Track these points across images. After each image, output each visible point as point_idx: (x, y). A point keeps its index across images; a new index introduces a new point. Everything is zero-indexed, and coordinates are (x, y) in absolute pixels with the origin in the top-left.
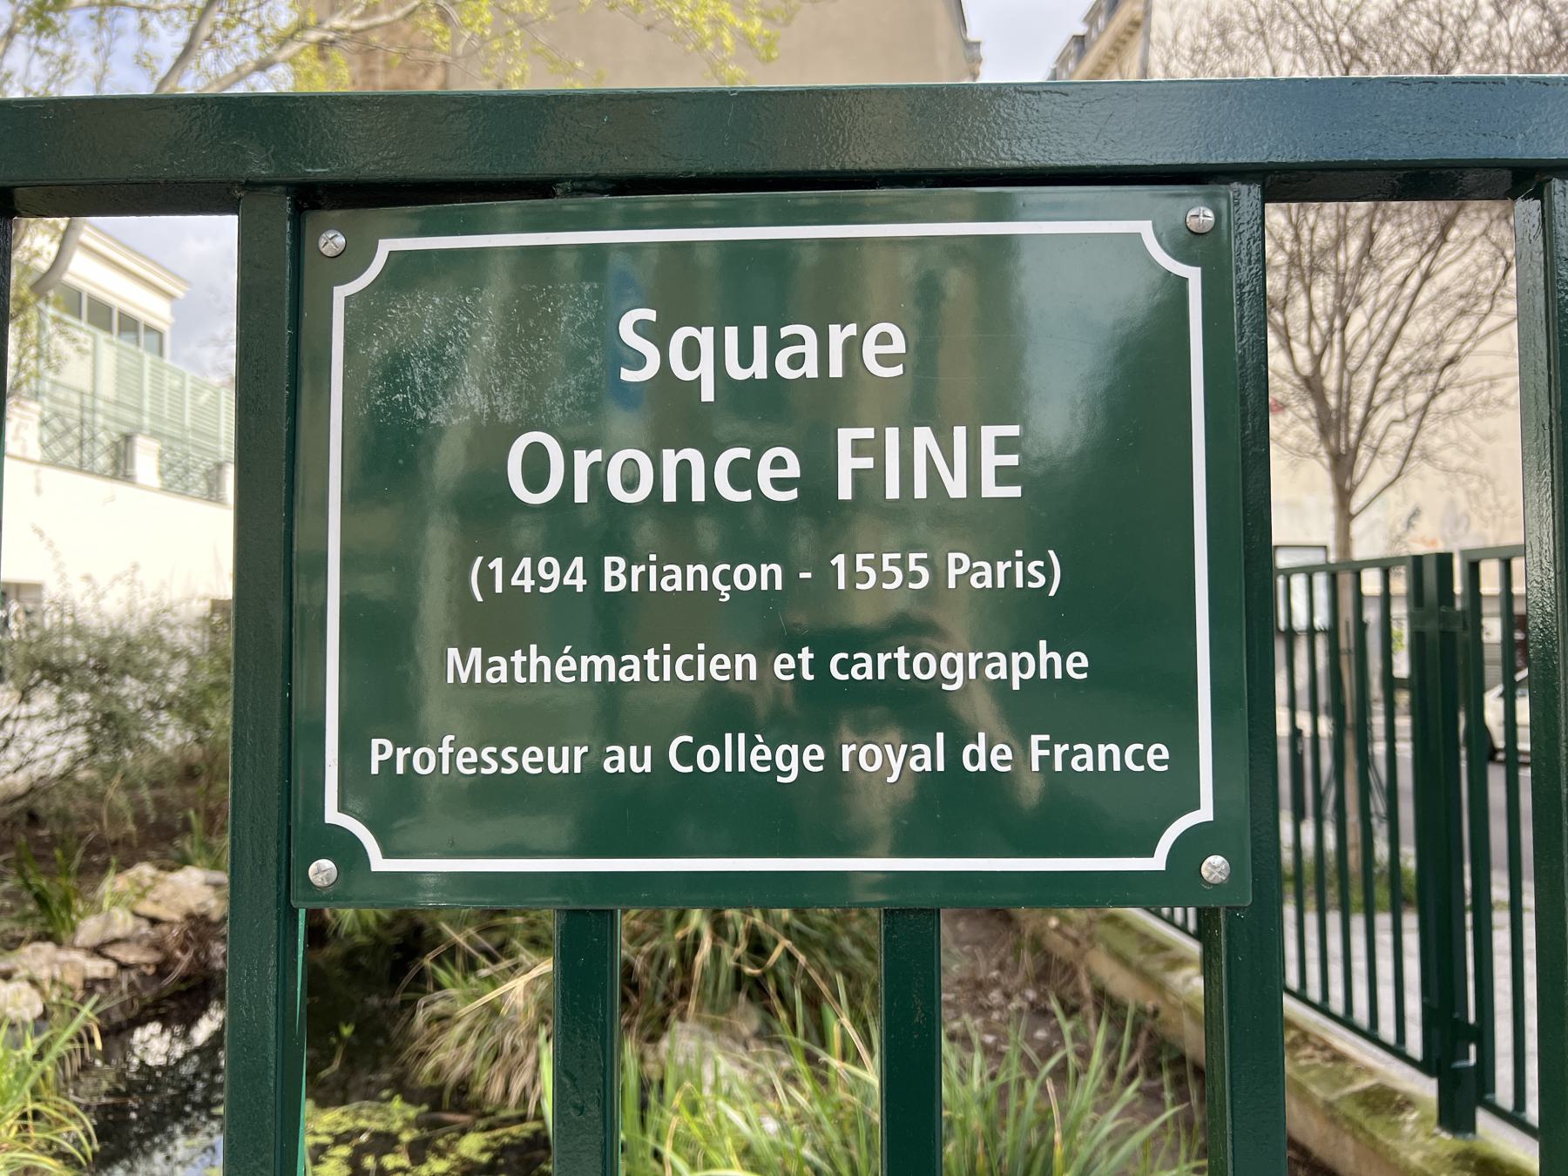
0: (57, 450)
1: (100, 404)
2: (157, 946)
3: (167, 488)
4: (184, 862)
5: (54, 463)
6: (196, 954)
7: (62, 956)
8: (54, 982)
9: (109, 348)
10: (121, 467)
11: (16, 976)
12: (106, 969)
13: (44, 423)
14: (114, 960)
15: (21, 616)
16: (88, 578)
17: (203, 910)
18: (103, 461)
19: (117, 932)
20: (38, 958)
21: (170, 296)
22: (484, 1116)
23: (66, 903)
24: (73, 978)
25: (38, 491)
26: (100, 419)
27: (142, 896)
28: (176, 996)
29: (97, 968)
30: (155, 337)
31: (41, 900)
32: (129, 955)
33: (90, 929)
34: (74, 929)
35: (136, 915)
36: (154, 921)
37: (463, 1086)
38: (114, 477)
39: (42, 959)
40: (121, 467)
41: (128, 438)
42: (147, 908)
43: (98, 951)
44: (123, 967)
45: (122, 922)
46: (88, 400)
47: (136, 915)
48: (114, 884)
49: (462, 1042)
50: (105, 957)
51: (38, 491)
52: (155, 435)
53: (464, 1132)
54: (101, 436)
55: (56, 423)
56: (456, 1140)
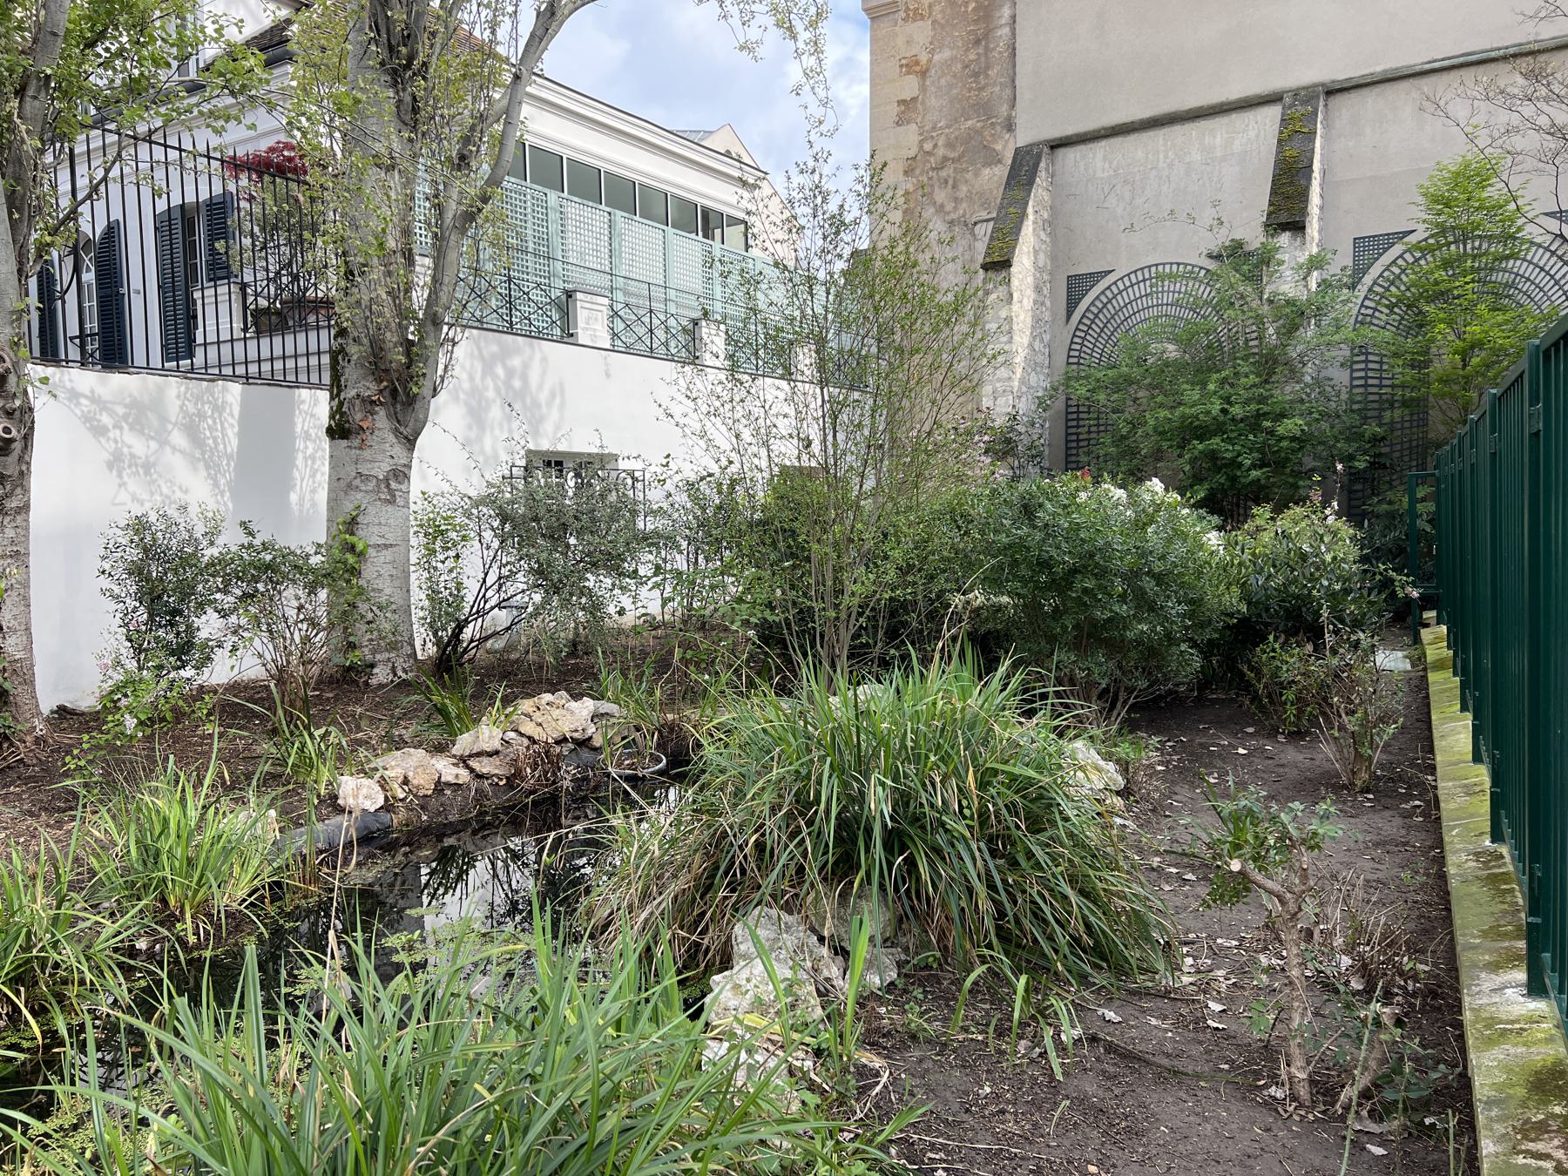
25: (608, 375)
33: (464, 744)
44: (480, 776)
46: (658, 293)
51: (608, 375)
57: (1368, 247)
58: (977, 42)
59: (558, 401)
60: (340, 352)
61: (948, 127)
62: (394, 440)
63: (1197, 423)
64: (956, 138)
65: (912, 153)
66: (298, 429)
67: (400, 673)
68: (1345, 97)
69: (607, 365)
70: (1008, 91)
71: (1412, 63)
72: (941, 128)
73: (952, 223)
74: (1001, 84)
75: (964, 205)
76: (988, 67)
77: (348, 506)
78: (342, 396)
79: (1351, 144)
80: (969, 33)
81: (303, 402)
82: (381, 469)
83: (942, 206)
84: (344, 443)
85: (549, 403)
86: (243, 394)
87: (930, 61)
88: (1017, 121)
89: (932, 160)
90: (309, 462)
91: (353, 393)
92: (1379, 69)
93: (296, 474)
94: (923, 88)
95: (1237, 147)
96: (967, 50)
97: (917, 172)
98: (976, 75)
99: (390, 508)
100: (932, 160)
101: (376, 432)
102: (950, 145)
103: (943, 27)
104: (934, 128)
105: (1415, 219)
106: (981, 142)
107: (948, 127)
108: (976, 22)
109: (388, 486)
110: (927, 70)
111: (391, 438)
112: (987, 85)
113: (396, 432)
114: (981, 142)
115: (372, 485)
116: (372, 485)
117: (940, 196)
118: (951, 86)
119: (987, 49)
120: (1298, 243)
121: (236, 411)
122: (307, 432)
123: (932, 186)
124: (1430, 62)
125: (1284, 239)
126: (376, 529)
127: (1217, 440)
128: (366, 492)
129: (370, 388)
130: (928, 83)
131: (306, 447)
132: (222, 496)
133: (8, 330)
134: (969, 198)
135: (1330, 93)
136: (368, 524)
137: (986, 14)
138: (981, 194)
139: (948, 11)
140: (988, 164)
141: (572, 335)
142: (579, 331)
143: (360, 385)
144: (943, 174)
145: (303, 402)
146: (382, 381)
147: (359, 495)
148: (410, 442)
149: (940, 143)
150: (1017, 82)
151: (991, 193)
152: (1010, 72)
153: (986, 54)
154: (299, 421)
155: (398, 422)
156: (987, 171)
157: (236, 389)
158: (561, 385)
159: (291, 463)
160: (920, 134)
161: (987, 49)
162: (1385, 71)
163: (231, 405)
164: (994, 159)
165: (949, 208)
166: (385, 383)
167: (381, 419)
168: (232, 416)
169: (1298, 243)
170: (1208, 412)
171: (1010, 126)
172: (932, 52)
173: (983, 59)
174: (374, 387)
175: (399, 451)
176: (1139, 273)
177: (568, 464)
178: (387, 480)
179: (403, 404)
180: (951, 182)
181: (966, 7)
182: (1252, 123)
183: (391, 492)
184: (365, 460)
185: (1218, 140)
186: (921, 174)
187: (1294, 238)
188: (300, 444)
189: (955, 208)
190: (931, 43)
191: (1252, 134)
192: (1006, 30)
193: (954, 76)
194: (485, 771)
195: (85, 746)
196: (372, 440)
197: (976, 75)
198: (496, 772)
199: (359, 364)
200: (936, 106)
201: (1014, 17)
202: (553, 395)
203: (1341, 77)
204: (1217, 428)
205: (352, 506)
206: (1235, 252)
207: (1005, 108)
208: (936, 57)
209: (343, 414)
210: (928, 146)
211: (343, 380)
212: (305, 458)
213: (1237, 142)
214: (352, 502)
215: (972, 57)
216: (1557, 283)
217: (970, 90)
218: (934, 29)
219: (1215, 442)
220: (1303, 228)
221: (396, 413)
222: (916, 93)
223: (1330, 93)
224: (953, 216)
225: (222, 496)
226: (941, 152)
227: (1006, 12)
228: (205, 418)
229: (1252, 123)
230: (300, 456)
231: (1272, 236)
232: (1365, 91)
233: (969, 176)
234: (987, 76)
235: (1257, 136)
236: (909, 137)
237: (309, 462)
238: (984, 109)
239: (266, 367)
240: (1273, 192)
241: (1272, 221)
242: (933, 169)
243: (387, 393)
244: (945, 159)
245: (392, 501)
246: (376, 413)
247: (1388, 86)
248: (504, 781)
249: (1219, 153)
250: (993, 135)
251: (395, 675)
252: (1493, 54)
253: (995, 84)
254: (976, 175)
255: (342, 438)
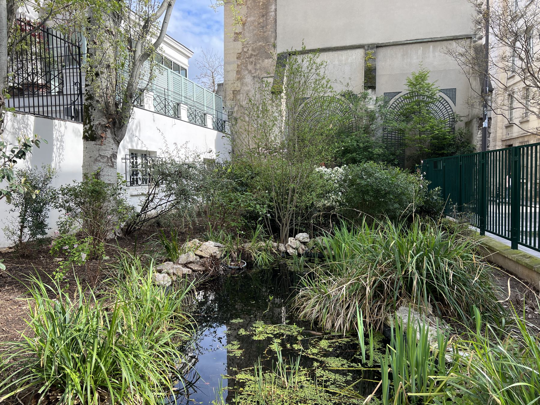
0: (159, 108)
1: (170, 93)
2: (203, 265)
3: (190, 122)
4: (207, 240)
5: (158, 113)
6: (215, 268)
7: (175, 266)
8: (174, 274)
9: (170, 73)
10: (177, 116)
11: (163, 272)
12: (189, 271)
13: (155, 99)
14: (191, 268)
15: (151, 162)
16: (175, 144)
17: (215, 254)
18: (172, 112)
19: (191, 260)
20: (168, 266)
21: (189, 57)
22: (326, 334)
23: (175, 249)
24: (180, 274)
25: (154, 121)
26: (170, 98)
27: (197, 249)
28: (210, 281)
29: (186, 271)
30: (185, 71)
31: (167, 247)
32: (196, 268)
33: (183, 258)
34: (178, 258)
35: (196, 255)
36: (201, 257)
37: (316, 322)
38: (174, 118)
39: (169, 267)
40: (177, 116)
41: (178, 105)
42: (198, 252)
43: (185, 265)
44: (194, 271)
45: (192, 257)
46: (166, 91)
47: (196, 255)
48: (189, 244)
49: (314, 306)
50: (188, 267)
51: (154, 121)
52: (186, 104)
53: (321, 339)
54: (170, 104)
55: (158, 99)
56: (318, 341)
57: (389, 95)
58: (263, 16)
59: (138, 128)
60: (90, 106)
61: (253, 44)
62: (113, 142)
63: (349, 148)
64: (256, 48)
65: (239, 52)
66: (54, 136)
67: (117, 234)
68: (384, 49)
69: (154, 117)
70: (274, 34)
71: (401, 40)
72: (250, 44)
73: (254, 77)
74: (271, 31)
75: (259, 71)
76: (267, 25)
77: (95, 168)
78: (92, 124)
79: (383, 64)
80: (260, 12)
81: (56, 125)
82: (109, 154)
83: (251, 71)
84: (93, 142)
85: (136, 129)
86: (35, 121)
87: (246, 20)
88: (277, 44)
89: (247, 54)
90: (58, 150)
91: (97, 123)
92: (391, 41)
93: (54, 155)
94: (244, 29)
95: (349, 61)
96: (260, 18)
97: (242, 58)
98: (263, 27)
99: (112, 169)
100: (247, 54)
101: (107, 139)
102: (253, 50)
103: (251, 9)
104: (247, 44)
105: (405, 89)
106: (265, 50)
107: (253, 44)
108: (263, 9)
109: (111, 160)
110: (245, 23)
111: (112, 141)
112: (267, 31)
113: (114, 139)
114: (265, 50)
115: (106, 159)
116: (106, 159)
117: (250, 67)
118: (254, 30)
119: (266, 19)
120: (374, 93)
121: (32, 128)
122: (57, 138)
123: (247, 63)
124: (406, 41)
125: (370, 91)
126: (107, 177)
127: (355, 154)
128: (103, 162)
129: (104, 121)
130: (245, 28)
131: (57, 144)
132: (27, 163)
133: (2, 85)
134: (260, 69)
135: (377, 47)
136: (104, 175)
137: (266, 6)
138: (264, 68)
139: (253, 4)
140: (267, 58)
141: (142, 106)
142: (145, 104)
143: (98, 120)
144: (251, 60)
145: (56, 125)
146: (109, 119)
147: (100, 164)
148: (118, 143)
149: (250, 49)
150: (277, 32)
151: (268, 68)
152: (275, 27)
153: (266, 21)
154: (54, 133)
155: (115, 135)
156: (266, 60)
157: (31, 119)
158: (139, 123)
159: (52, 151)
160: (243, 45)
161: (266, 19)
162: (393, 42)
163: (30, 125)
164: (269, 56)
165: (253, 72)
166: (111, 120)
167: (109, 134)
168: (31, 130)
169: (374, 93)
170: (353, 145)
171: (275, 46)
172: (247, 17)
173: (265, 22)
174: (106, 120)
175: (114, 146)
176: (445, 102)
177: (139, 154)
178: (111, 158)
179: (118, 128)
180: (254, 63)
181: (259, 3)
182: (354, 54)
183: (112, 163)
184: (102, 150)
185: (343, 58)
186: (243, 58)
187: (372, 91)
188: (55, 143)
189: (255, 72)
190: (246, 14)
191: (354, 57)
192: (273, 13)
193: (255, 26)
194: (196, 269)
195: (62, 267)
196: (105, 142)
197: (263, 27)
198: (200, 269)
199: (100, 111)
200: (248, 37)
201: (276, 9)
202: (137, 126)
203: (380, 42)
204: (355, 150)
205: (97, 168)
206: (350, 96)
207: (273, 40)
208: (249, 19)
209: (92, 131)
210: (245, 50)
211: (92, 117)
212: (57, 148)
213: (349, 59)
214: (97, 166)
215: (261, 21)
216: (441, 110)
217: (261, 32)
218: (247, 9)
219: (354, 154)
220: (375, 88)
221: (114, 132)
222: (241, 31)
223: (377, 47)
224: (255, 75)
225: (27, 163)
226: (250, 52)
227: (273, 7)
228: (21, 129)
229: (354, 54)
230: (55, 147)
231: (366, 90)
232: (387, 48)
233: (260, 61)
234: (267, 28)
235: (356, 58)
236: (238, 46)
237: (58, 150)
238: (266, 39)
239: (36, 109)
240: (365, 76)
241: (366, 85)
242: (247, 58)
243: (111, 123)
244: (252, 55)
245: (112, 166)
246: (107, 131)
247: (394, 47)
248: (202, 273)
249: (344, 62)
250: (268, 48)
251: (116, 235)
252: (408, 42)
253: (269, 31)
254: (263, 61)
255: (93, 141)
